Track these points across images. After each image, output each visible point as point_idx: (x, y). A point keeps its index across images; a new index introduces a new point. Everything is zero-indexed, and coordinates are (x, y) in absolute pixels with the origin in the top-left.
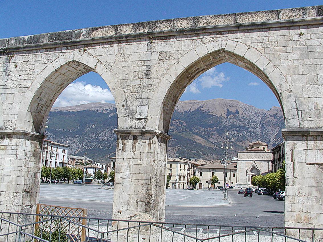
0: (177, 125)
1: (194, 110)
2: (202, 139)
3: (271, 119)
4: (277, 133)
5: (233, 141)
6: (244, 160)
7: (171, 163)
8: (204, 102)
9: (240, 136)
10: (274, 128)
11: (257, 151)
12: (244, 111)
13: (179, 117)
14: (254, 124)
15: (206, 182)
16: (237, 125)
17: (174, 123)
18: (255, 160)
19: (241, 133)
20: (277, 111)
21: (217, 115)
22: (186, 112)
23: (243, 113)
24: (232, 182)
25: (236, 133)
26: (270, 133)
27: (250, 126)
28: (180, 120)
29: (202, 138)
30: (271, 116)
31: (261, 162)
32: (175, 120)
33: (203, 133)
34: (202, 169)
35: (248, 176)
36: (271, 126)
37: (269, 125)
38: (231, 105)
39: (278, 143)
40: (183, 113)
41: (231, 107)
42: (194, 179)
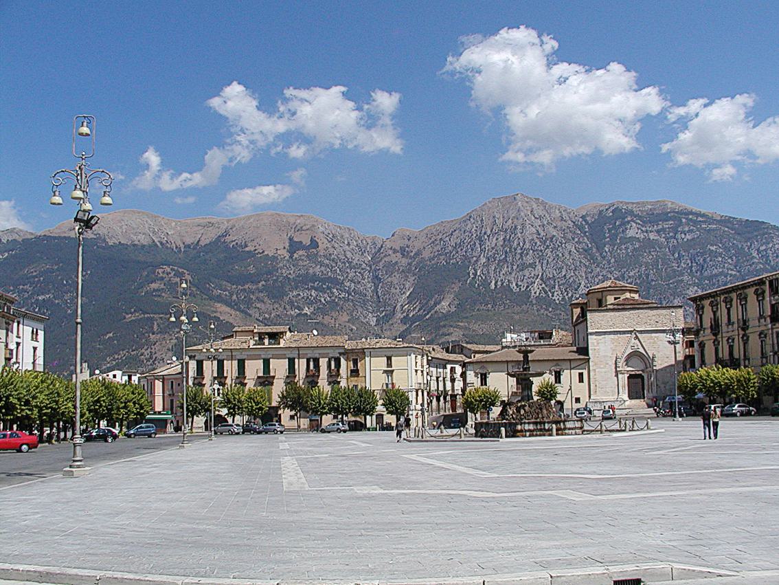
0: (170, 280)
1: (208, 242)
2: (233, 312)
3: (395, 258)
4: (410, 291)
5: (309, 314)
6: (605, 333)
7: (389, 354)
8: (232, 221)
9: (325, 300)
10: (403, 280)
11: (641, 306)
12: (330, 240)
13: (173, 259)
14: (355, 272)
15: (576, 402)
16: (315, 275)
17: (161, 275)
18: (638, 331)
19: (325, 293)
20: (409, 240)
21: (266, 253)
22: (190, 248)
23: (328, 245)
24: (575, 396)
25: (314, 295)
26: (393, 290)
27: (347, 277)
28: (176, 268)
29: (233, 308)
30: (395, 251)
31: (653, 335)
32: (164, 267)
33: (234, 297)
34: (485, 365)
35: (620, 376)
36: (396, 274)
37: (392, 274)
38: (298, 227)
39: (413, 315)
40: (183, 250)
41: (299, 232)
42: (485, 395)
